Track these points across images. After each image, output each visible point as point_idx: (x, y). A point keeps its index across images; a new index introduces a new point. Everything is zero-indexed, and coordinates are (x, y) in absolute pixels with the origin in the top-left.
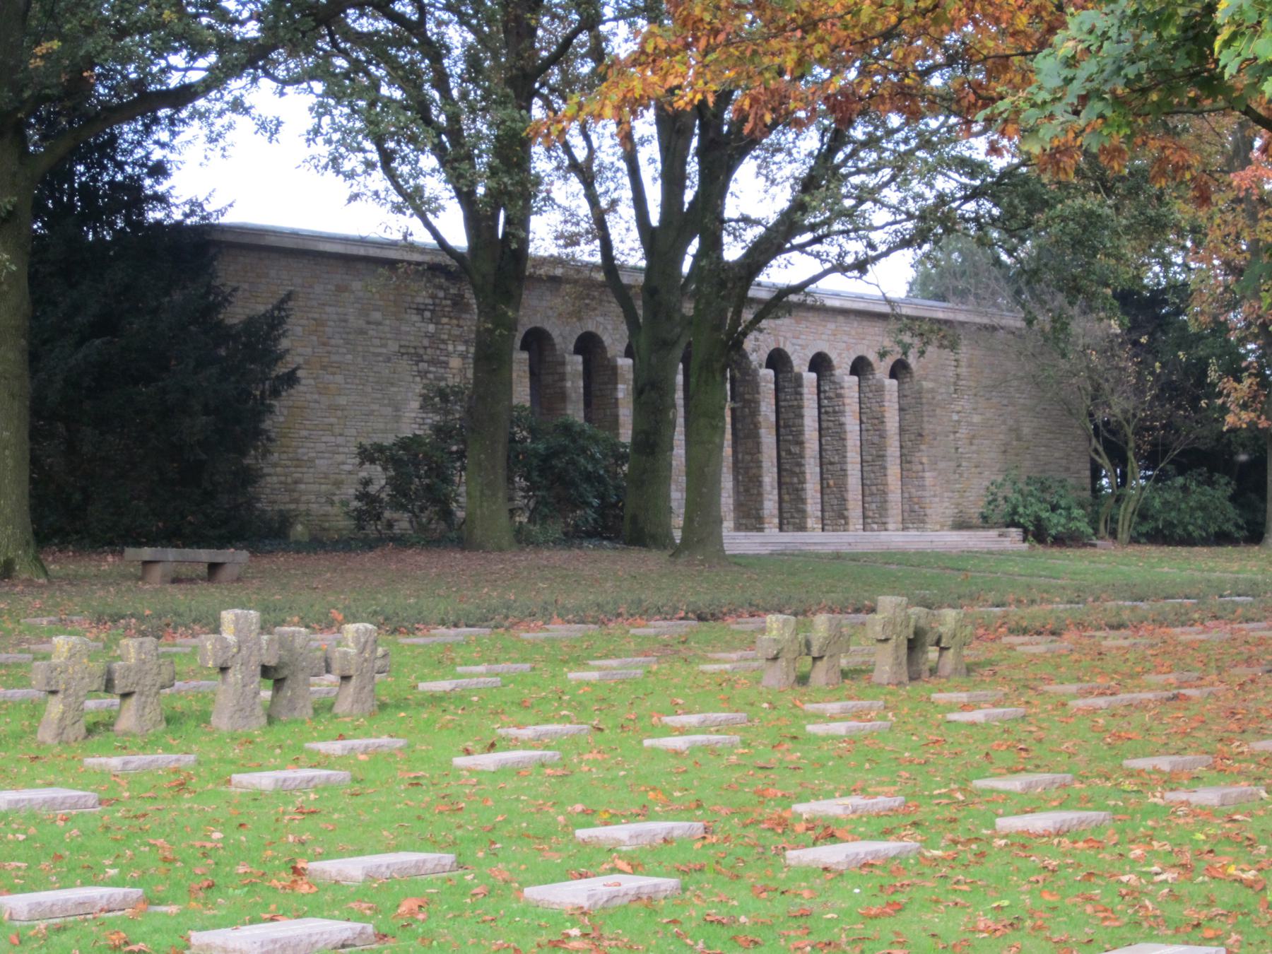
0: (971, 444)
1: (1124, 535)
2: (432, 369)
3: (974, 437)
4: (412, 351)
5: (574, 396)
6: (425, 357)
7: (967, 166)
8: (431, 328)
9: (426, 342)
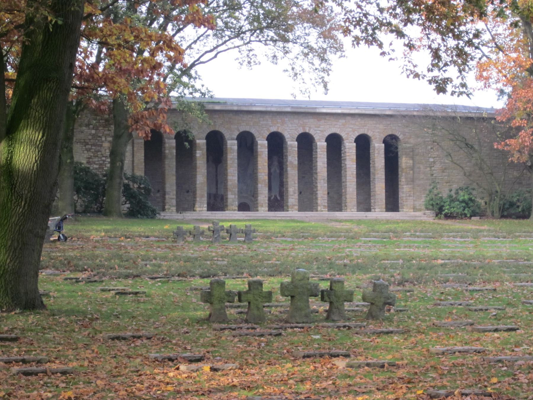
0: (443, 172)
1: (497, 214)
2: (93, 148)
3: (445, 169)
4: (83, 141)
5: (170, 156)
6: (90, 143)
7: (172, 49)
8: (93, 132)
9: (90, 137)
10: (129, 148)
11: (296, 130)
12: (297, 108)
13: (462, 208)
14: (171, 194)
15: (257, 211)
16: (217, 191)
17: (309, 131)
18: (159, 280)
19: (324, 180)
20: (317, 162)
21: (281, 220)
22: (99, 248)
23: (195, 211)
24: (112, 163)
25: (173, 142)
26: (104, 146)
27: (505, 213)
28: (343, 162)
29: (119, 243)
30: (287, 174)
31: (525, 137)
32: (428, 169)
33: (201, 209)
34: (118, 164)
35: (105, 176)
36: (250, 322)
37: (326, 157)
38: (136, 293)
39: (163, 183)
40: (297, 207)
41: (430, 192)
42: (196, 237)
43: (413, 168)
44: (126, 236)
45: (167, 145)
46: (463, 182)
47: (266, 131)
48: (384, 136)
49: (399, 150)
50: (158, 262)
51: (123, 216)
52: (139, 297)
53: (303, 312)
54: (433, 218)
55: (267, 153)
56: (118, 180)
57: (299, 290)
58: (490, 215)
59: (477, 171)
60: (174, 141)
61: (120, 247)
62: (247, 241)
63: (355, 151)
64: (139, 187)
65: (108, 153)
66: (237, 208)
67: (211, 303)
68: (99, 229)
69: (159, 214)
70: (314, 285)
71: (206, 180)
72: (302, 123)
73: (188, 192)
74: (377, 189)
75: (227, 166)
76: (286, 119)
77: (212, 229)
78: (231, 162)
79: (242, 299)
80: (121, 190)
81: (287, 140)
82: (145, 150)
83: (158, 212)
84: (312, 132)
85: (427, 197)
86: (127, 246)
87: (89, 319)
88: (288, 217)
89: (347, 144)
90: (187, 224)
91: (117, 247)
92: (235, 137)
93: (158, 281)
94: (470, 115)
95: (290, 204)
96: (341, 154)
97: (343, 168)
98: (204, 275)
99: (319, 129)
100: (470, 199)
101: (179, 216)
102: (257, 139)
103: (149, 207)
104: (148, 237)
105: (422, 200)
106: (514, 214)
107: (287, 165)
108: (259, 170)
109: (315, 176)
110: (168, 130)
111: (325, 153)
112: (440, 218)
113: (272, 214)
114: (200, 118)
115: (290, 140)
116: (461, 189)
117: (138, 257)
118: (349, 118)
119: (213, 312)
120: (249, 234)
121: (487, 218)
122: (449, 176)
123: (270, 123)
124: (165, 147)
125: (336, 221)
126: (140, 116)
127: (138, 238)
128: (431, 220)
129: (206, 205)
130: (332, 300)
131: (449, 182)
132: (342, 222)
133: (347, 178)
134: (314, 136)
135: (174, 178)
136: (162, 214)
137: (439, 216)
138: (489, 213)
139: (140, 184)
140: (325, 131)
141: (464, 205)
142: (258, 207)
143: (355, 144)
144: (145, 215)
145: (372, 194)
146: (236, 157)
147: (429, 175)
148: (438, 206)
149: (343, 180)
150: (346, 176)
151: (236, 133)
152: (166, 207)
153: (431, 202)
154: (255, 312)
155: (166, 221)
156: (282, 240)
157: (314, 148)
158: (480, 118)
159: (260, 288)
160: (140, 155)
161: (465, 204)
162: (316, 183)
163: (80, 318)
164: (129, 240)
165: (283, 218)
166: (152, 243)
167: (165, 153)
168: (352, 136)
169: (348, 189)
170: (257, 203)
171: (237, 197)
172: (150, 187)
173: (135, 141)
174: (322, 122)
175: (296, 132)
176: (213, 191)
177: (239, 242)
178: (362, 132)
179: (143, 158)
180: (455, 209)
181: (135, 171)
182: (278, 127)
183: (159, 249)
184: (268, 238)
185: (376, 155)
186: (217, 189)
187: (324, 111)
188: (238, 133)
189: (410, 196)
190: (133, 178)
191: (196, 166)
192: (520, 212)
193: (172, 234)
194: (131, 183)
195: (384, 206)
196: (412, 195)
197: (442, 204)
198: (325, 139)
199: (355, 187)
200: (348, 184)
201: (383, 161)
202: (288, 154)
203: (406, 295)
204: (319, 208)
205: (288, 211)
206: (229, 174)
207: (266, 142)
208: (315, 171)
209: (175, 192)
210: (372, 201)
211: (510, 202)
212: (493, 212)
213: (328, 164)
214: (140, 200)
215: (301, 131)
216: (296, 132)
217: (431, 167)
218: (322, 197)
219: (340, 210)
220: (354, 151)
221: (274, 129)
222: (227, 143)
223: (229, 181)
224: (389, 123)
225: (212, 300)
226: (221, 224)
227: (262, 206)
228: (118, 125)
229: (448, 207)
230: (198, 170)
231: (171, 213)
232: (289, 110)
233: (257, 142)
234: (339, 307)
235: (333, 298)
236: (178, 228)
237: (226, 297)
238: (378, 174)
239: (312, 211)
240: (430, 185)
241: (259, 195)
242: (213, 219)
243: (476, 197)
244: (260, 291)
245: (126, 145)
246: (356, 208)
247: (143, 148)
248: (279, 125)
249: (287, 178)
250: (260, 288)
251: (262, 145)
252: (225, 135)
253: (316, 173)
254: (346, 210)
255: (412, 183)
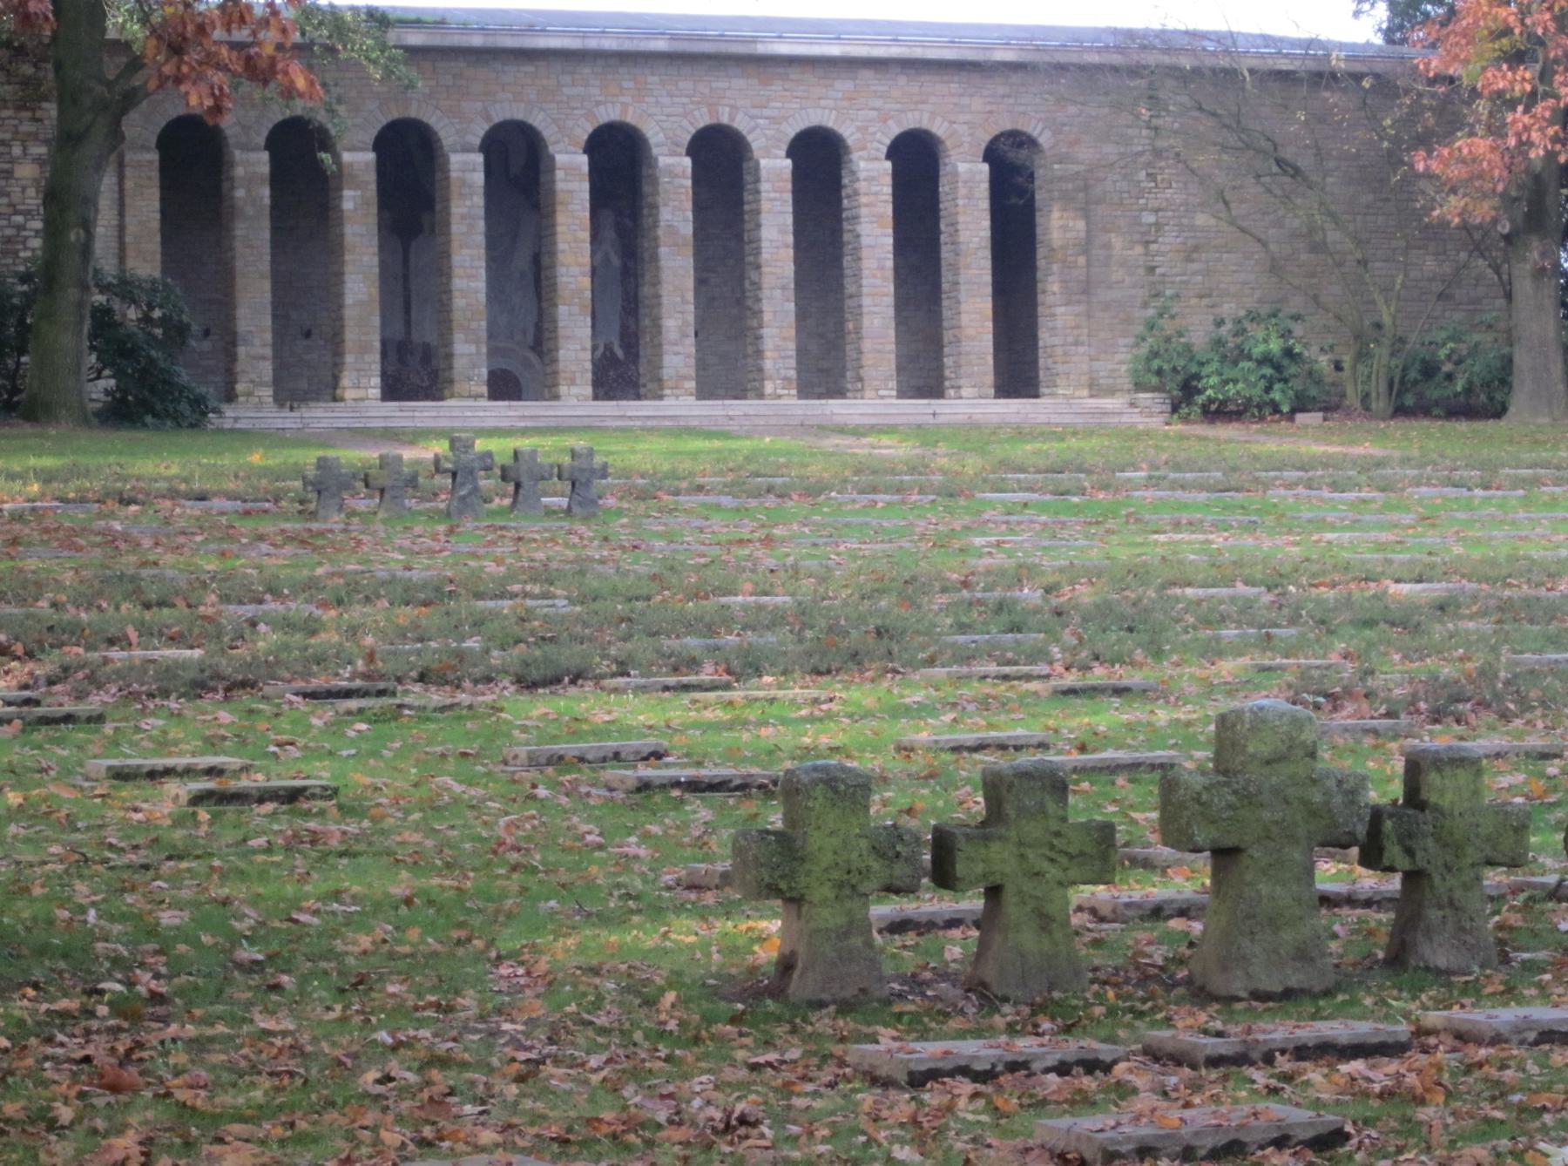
0: (1189, 260)
1: (1380, 404)
3: (1196, 248)
5: (250, 211)
10: (108, 182)
11: (685, 115)
12: (689, 38)
13: (1263, 383)
14: (257, 341)
15: (556, 397)
16: (408, 333)
17: (732, 118)
18: (353, 704)
19: (784, 288)
20: (758, 226)
21: (651, 430)
22: (30, 544)
23: (342, 400)
24: (53, 232)
25: (261, 162)
26: (17, 175)
27: (1409, 400)
28: (846, 226)
29: (103, 523)
30: (658, 268)
31: (1526, 128)
32: (1139, 249)
33: (360, 393)
34: (73, 237)
35: (25, 278)
36: (1005, 1000)
37: (790, 209)
38: (292, 796)
39: (224, 303)
40: (691, 385)
41: (1151, 327)
42: (387, 496)
43: (1086, 247)
44: (121, 493)
45: (239, 171)
46: (1258, 294)
47: (618, 108)
48: (988, 138)
49: (1037, 183)
50: (299, 608)
51: (95, 421)
52: (307, 814)
53: (1287, 936)
54: (1161, 419)
55: (587, 196)
56: (73, 294)
57: (1266, 815)
58: (1357, 404)
59: (1304, 257)
60: (265, 156)
61: (111, 540)
62: (576, 509)
63: (888, 190)
64: (147, 319)
65: (33, 199)
66: (484, 390)
67: (795, 901)
68: (17, 468)
69: (217, 411)
70: (1340, 783)
71: (375, 291)
72: (706, 91)
73: (308, 334)
74: (965, 320)
75: (449, 242)
76: (651, 79)
77: (449, 466)
78: (464, 229)
79: (960, 868)
80: (85, 331)
81: (655, 151)
82: (163, 188)
83: (212, 403)
84: (741, 124)
85: (1137, 345)
86: (135, 532)
87: (117, 1008)
88: (664, 417)
89: (862, 164)
90: (412, 443)
91: (98, 539)
92: (477, 141)
93: (349, 713)
94: (1284, 65)
95: (667, 373)
96: (839, 200)
97: (847, 249)
98: (535, 675)
99: (767, 112)
100: (1289, 353)
101: (287, 420)
102: (551, 149)
103: (182, 389)
104: (202, 497)
105: (1118, 357)
106: (1437, 403)
107: (656, 239)
108: (561, 257)
109: (753, 275)
110: (301, 83)
111: (789, 197)
112: (1186, 420)
113: (608, 408)
114: (375, 62)
115: (665, 150)
116: (1254, 317)
117: (204, 585)
118: (867, 74)
119: (801, 949)
120: (588, 484)
121: (1348, 415)
122: (1208, 273)
123: (596, 91)
124: (231, 179)
125: (842, 430)
126: (190, 28)
127: (168, 503)
128: (1156, 422)
129: (376, 381)
130: (1421, 862)
131: (1210, 296)
132: (864, 435)
133: (864, 282)
134: (750, 138)
135: (267, 285)
136: (229, 411)
137: (1184, 410)
138: (1353, 399)
139: (151, 307)
140: (785, 119)
141: (1268, 371)
142: (556, 385)
143: (888, 165)
144: (168, 415)
145: (948, 336)
146: (481, 212)
147: (1141, 271)
148: (1179, 378)
149: (850, 288)
150: (857, 276)
151: (479, 130)
152: (240, 387)
153: (1156, 364)
154: (1028, 940)
155: (248, 437)
156: (704, 505)
157: (748, 178)
158: (1320, 75)
159: (1051, 807)
160: (146, 207)
161: (1279, 366)
162: (759, 300)
163: (64, 1004)
164: (133, 508)
165: (649, 423)
166: (224, 520)
167: (232, 198)
168: (879, 136)
169: (866, 322)
170: (556, 373)
171: (484, 350)
172: (185, 318)
173: (128, 157)
174: (777, 86)
175: (685, 123)
176: (398, 330)
177: (550, 512)
178: (911, 121)
179: (158, 216)
180: (1240, 386)
181: (130, 263)
182: (625, 106)
183: (264, 547)
184: (643, 496)
185: (960, 202)
186: (408, 323)
187: (783, 49)
188: (487, 127)
189: (1076, 343)
190: (125, 288)
191: (341, 245)
192: (1457, 395)
193: (298, 484)
194: (116, 305)
195: (990, 378)
196: (1084, 338)
197: (1194, 369)
198: (785, 147)
199: (891, 312)
200: (866, 301)
201: (987, 223)
202: (660, 200)
203: (1542, 775)
204: (769, 387)
205: (661, 397)
206: (457, 271)
207: (585, 159)
208: (751, 259)
209: (268, 336)
210: (948, 361)
211: (1423, 361)
212: (1366, 397)
213: (799, 231)
214: (152, 361)
215: (703, 120)
216: (685, 123)
217: (1147, 243)
218: (777, 348)
219: (840, 393)
220: (886, 189)
221: (609, 113)
222: (447, 162)
223: (456, 294)
224: (1001, 90)
225: (803, 880)
226: (480, 445)
227: (572, 382)
228: (68, 98)
229: (1214, 380)
230: (347, 257)
231: (260, 405)
232: (661, 45)
233: (552, 159)
234: (1458, 893)
235: (1430, 853)
236: (322, 463)
237: (876, 866)
238: (968, 267)
239: (745, 398)
240: (1145, 305)
241: (562, 342)
242: (453, 429)
243: (1306, 346)
244: (1054, 825)
245: (99, 168)
246: (893, 384)
247: (156, 182)
248: (628, 99)
249: (656, 282)
250: (1051, 807)
251: (571, 170)
252: (442, 134)
253: (758, 267)
254: (859, 393)
255: (1084, 298)
